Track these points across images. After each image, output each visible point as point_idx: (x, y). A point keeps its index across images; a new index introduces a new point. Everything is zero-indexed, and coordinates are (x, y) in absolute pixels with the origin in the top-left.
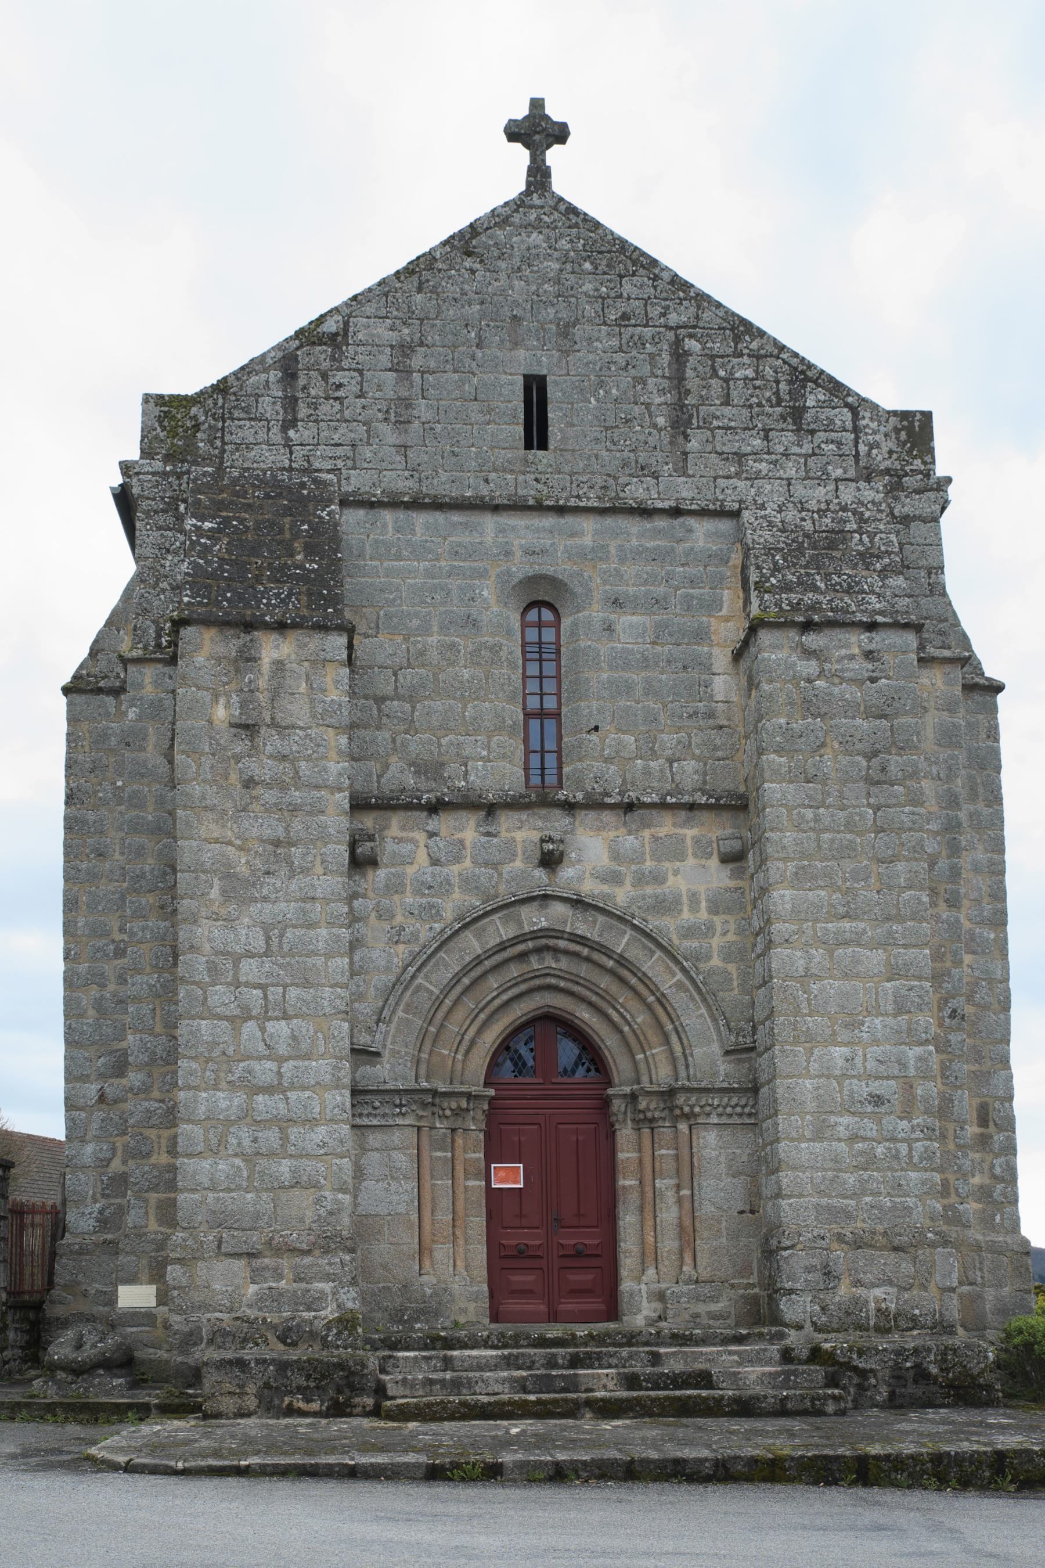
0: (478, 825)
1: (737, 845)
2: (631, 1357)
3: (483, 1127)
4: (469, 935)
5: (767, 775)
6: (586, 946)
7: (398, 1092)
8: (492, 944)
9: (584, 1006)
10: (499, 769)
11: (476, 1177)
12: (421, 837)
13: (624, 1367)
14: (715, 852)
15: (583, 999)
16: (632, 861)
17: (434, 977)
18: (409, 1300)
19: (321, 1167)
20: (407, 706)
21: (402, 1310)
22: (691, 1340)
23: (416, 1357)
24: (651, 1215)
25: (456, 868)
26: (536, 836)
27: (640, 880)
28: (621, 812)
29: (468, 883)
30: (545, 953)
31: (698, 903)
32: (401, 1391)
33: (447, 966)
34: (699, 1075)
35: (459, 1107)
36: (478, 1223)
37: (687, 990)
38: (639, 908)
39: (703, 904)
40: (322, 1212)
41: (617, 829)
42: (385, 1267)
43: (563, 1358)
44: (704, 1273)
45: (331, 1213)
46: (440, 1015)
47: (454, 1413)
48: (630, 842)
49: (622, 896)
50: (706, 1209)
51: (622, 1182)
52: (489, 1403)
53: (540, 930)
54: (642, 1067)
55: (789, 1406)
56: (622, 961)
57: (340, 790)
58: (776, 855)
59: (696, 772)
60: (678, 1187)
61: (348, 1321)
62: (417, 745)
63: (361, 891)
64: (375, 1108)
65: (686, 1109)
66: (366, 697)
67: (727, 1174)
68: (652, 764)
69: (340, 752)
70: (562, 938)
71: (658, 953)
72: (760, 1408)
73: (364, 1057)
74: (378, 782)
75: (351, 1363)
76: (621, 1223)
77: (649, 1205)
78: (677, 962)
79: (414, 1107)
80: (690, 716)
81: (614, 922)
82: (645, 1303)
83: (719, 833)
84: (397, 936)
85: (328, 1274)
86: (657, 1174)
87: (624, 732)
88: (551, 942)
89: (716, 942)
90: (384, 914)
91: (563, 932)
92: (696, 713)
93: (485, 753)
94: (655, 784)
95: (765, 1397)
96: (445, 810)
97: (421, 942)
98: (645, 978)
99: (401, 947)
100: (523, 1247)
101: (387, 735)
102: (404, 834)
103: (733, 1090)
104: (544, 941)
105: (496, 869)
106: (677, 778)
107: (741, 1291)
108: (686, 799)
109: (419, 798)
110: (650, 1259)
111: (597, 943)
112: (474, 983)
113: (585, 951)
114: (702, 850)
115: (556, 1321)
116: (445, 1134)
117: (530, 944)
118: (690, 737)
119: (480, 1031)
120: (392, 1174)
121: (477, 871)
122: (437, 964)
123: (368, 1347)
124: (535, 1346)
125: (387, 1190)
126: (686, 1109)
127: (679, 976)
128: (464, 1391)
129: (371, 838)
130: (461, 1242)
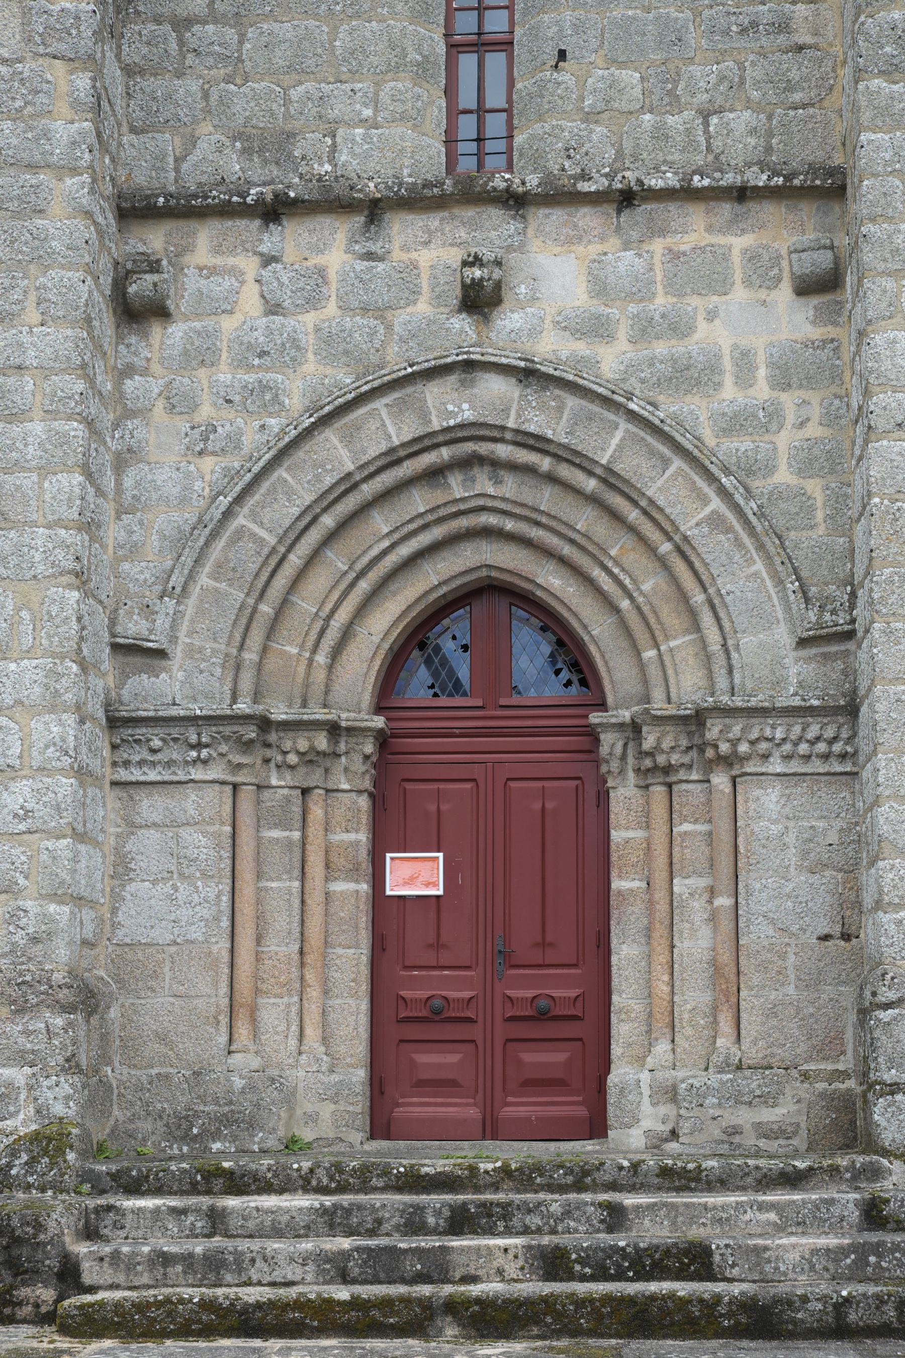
0: (352, 241)
1: (824, 259)
2: (567, 1213)
3: (367, 784)
4: (330, 436)
5: (866, 117)
6: (546, 453)
7: (192, 720)
8: (373, 452)
9: (551, 565)
10: (397, 141)
11: (353, 873)
12: (249, 265)
13: (554, 1232)
14: (786, 275)
15: (549, 553)
16: (630, 297)
17: (267, 515)
18: (202, 1099)
19: (19, 854)
20: (231, 34)
21: (189, 1119)
22: (698, 1180)
23: (157, 1211)
24: (665, 943)
25: (310, 319)
26: (455, 256)
27: (644, 330)
28: (611, 209)
29: (331, 343)
30: (476, 470)
31: (752, 369)
32: (107, 1275)
33: (290, 493)
34: (749, 685)
35: (312, 748)
36: (352, 959)
37: (729, 529)
38: (643, 381)
39: (762, 372)
40: (19, 937)
41: (603, 239)
42: (162, 1038)
43: (438, 1213)
44: (752, 1052)
45: (35, 940)
46: (281, 582)
47: (188, 1322)
48: (626, 262)
49: (610, 361)
50: (758, 933)
51: (618, 884)
52: (258, 1306)
53: (461, 426)
54: (654, 672)
55: (852, 1317)
56: (611, 479)
57: (74, 171)
58: (881, 266)
59: (753, 132)
60: (712, 892)
61: (50, 1139)
62: (246, 102)
63: (139, 362)
64: (154, 751)
65: (724, 748)
66: (158, 20)
67: (799, 868)
68: (670, 120)
69: (76, 104)
70: (502, 440)
71: (677, 463)
72: (794, 1322)
73: (138, 660)
74: (177, 170)
75: (15, 1222)
76: (614, 959)
77: (666, 925)
78: (711, 478)
79: (224, 748)
80: (743, 31)
81: (595, 408)
82: (646, 1106)
83: (794, 239)
84: (203, 442)
85: (23, 1052)
86: (676, 867)
87: (622, 65)
88: (483, 448)
89: (785, 440)
90: (178, 403)
91: (503, 428)
92: (754, 24)
93: (368, 112)
94: (676, 157)
95: (805, 1299)
96: (293, 215)
97: (246, 451)
98: (651, 511)
99: (208, 463)
100: (437, 1002)
101: (194, 86)
102: (218, 261)
103: (811, 711)
104: (469, 447)
105: (383, 318)
106: (717, 144)
107: (821, 1086)
108: (729, 179)
109: (243, 195)
110: (661, 1023)
111: (565, 447)
112: (343, 525)
113: (545, 464)
114: (761, 271)
115: (494, 1138)
116: (288, 800)
117: (445, 453)
118: (742, 68)
119: (361, 611)
120: (182, 869)
121: (348, 322)
122: (272, 490)
123: (86, 1188)
124: (399, 1189)
125: (172, 899)
126: (724, 748)
127: (716, 503)
128: (229, 1278)
129: (154, 267)
130: (314, 993)
